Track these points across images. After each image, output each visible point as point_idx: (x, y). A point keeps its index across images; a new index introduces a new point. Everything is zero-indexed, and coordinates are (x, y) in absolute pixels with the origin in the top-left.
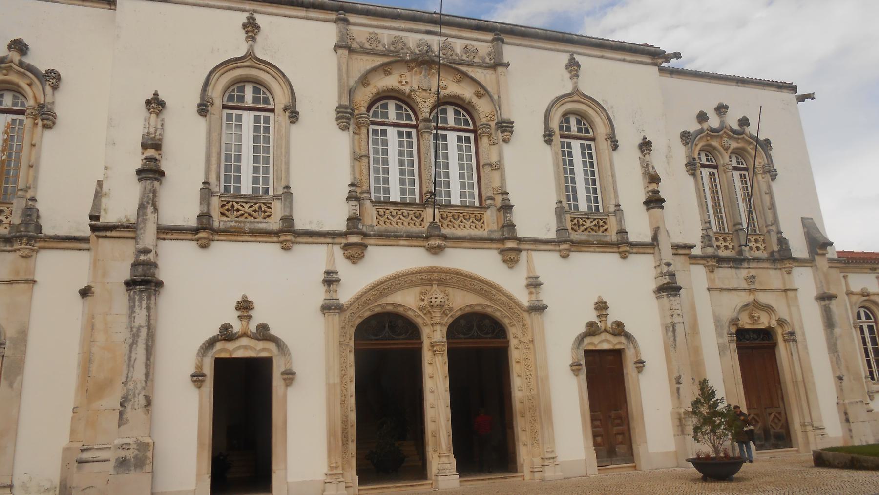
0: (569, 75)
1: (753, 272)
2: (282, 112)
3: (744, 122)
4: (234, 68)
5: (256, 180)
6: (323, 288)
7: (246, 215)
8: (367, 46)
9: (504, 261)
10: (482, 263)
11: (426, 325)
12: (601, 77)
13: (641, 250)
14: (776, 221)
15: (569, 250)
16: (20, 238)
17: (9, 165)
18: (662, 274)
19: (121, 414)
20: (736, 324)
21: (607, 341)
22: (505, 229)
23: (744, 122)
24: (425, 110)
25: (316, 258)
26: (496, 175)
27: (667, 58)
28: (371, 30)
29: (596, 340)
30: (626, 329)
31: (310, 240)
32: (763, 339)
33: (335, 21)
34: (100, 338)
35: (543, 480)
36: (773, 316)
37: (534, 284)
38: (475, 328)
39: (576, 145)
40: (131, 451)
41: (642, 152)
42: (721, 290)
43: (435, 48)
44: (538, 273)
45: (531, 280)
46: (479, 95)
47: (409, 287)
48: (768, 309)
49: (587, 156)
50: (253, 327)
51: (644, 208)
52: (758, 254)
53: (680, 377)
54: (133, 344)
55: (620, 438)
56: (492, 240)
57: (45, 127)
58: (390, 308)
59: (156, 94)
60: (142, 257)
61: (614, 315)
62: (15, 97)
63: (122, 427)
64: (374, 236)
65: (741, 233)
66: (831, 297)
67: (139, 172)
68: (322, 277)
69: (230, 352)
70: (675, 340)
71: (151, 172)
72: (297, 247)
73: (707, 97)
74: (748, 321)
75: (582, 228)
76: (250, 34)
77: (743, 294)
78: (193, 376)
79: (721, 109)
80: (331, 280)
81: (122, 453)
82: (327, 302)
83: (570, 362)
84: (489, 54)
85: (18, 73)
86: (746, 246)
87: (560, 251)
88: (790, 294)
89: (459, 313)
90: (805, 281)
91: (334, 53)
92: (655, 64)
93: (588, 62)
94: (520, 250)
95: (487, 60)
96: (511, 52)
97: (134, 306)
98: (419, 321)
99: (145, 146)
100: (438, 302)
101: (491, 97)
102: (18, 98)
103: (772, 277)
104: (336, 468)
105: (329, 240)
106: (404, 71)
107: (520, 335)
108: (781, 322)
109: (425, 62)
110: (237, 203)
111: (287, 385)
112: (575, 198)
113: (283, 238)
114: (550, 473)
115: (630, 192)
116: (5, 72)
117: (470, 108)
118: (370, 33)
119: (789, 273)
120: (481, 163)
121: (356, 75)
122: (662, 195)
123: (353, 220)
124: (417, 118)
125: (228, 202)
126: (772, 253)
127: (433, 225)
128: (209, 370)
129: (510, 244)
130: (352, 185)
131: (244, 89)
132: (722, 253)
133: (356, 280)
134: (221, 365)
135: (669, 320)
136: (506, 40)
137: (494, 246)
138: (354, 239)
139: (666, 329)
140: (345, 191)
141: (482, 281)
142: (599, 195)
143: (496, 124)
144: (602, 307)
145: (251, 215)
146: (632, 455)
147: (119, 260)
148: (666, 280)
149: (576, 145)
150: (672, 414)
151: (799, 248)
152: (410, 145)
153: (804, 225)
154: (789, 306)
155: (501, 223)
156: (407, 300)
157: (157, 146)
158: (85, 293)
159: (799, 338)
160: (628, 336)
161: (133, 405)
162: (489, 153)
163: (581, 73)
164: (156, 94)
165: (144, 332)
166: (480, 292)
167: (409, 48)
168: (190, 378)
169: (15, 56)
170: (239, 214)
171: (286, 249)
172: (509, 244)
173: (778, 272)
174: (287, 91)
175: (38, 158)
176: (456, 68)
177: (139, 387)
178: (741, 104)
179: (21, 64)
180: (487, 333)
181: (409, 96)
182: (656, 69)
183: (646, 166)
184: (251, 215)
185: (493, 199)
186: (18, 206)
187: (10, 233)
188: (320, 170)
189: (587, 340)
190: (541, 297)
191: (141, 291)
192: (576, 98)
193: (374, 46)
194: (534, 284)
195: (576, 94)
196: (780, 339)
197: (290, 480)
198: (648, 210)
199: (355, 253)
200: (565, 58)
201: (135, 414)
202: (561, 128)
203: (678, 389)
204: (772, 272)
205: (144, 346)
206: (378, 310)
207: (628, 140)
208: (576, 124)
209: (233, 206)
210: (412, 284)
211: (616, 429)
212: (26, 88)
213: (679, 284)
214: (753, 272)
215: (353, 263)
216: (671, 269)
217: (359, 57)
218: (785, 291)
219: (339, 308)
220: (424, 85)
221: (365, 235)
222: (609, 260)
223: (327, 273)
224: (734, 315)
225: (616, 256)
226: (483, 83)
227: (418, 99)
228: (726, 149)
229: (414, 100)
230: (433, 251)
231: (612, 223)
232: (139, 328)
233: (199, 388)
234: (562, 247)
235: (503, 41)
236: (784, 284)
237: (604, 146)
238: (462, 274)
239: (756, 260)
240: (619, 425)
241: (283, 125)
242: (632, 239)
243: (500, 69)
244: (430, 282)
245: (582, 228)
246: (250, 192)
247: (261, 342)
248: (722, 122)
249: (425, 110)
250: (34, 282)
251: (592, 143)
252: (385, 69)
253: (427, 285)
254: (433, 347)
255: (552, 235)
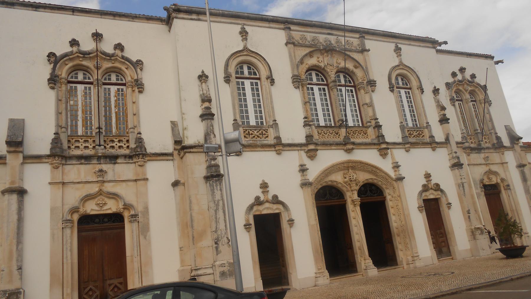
0: (396, 55)
1: (487, 155)
2: (266, 80)
3: (473, 76)
4: (239, 56)
5: (256, 117)
6: (299, 174)
7: (256, 137)
8: (301, 42)
9: (381, 155)
10: (369, 156)
11: (348, 191)
12: (412, 55)
13: (441, 146)
14: (494, 128)
15: (410, 147)
16: (138, 155)
17: (120, 115)
18: (453, 158)
19: (217, 248)
20: (482, 182)
21: (432, 194)
22: (380, 138)
23: (473, 76)
24: (332, 75)
25: (293, 159)
26: (370, 110)
27: (440, 44)
28: (301, 33)
29: (427, 193)
30: (279, 199)
31: (290, 148)
32: (114, 222)
33: (284, 29)
34: (195, 207)
35: (415, 268)
36: (498, 177)
37: (396, 166)
38: (369, 191)
39: (247, 83)
40: (226, 267)
41: (434, 95)
42: (474, 165)
43: (333, 42)
44: (397, 161)
45: (395, 164)
46: (356, 67)
47: (338, 171)
48: (496, 173)
49: (255, 89)
50: (270, 197)
51: (439, 124)
52: (487, 145)
53: (469, 210)
54: (216, 211)
55: (443, 244)
56: (374, 144)
57: (141, 92)
58: (330, 183)
59: (203, 72)
60: (213, 162)
61: (272, 191)
62: (84, 74)
63: (219, 255)
64: (321, 145)
65: (479, 134)
66: (524, 166)
67: (201, 116)
68: (298, 169)
69: (261, 211)
70: (464, 191)
71: (207, 116)
72: (283, 153)
73: (456, 63)
74: (487, 180)
75: (413, 136)
76: (244, 37)
77: (483, 166)
78: (245, 225)
79: (462, 70)
80: (303, 170)
81: (222, 269)
82: (304, 181)
83: (417, 206)
84: (359, 45)
85: (121, 62)
86: (482, 141)
87: (405, 148)
88: (505, 165)
89: (362, 184)
90: (510, 157)
91: (285, 46)
92: (434, 48)
93: (405, 48)
94: (317, 150)
95: (358, 48)
96: (369, 44)
97: (214, 189)
98: (344, 189)
99: (203, 101)
100: (354, 179)
101: (363, 68)
102: (118, 76)
103: (495, 157)
104: (321, 269)
105: (299, 148)
106: (319, 55)
107: (392, 193)
108: (503, 180)
109: (329, 50)
110: (251, 130)
111: (291, 227)
112: (248, 117)
113: (277, 148)
114: (418, 264)
115: (432, 116)
116: (113, 62)
117: (351, 74)
118: (301, 35)
119: (503, 154)
120: (361, 104)
121: (298, 59)
122: (448, 116)
123: (309, 137)
124: (327, 81)
125: (246, 130)
126: (493, 145)
127: (347, 138)
128: (252, 221)
129: (384, 146)
130: (305, 118)
131: (246, 68)
132: (472, 146)
133: (315, 169)
134: (256, 217)
135: (460, 181)
136: (366, 37)
137: (376, 147)
138: (312, 147)
139: (459, 186)
140: (302, 121)
141: (373, 166)
142: (417, 118)
143: (367, 82)
144: (428, 176)
145: (258, 137)
146: (450, 252)
147: (198, 164)
148: (456, 161)
149: (247, 83)
150: (466, 230)
151: (506, 142)
152: (325, 95)
153: (506, 129)
154: (505, 172)
155: (377, 134)
156: (338, 178)
157: (210, 101)
158: (176, 184)
159: (511, 187)
160: (442, 191)
161: (222, 243)
162: (365, 98)
163: (248, 38)
164: (203, 72)
165: (221, 203)
166: (370, 172)
167: (320, 43)
168: (243, 227)
169: (118, 52)
170: (258, 136)
171: (279, 154)
172: (382, 146)
173: (498, 154)
174: (267, 69)
175: (138, 111)
176: (344, 53)
177: (223, 233)
178: (473, 67)
179: (123, 57)
180: (374, 194)
181: (324, 69)
182: (434, 51)
183: (438, 102)
184: (258, 137)
185: (370, 122)
186: (132, 138)
187: (131, 153)
188: (289, 110)
189: (424, 194)
190: (401, 172)
191: (216, 181)
192: (401, 67)
193: (304, 42)
194: (396, 166)
195: (401, 65)
196: (502, 189)
197: (299, 278)
198: (441, 125)
199: (312, 155)
200: (238, 28)
201: (225, 249)
202: (237, 72)
203: (469, 217)
204: (495, 154)
205: (222, 211)
206: (324, 184)
207: (428, 89)
208: (403, 80)
209: (249, 132)
210: (340, 170)
211: (441, 239)
212: (125, 70)
213: (462, 162)
214: (487, 155)
215: (312, 160)
216: (457, 154)
217: (298, 48)
218: (502, 163)
219: (310, 184)
220: (330, 63)
221: (316, 144)
222: (269, 156)
223: (301, 166)
224: (481, 177)
225: (430, 150)
226: (359, 61)
227: (328, 70)
228: (466, 91)
229: (325, 71)
230: (348, 151)
231: (426, 132)
232: (218, 201)
233: (249, 232)
234: (407, 146)
235: (364, 37)
236: (63, 179)
237: (417, 92)
238: (363, 163)
239: (488, 148)
240: (442, 237)
241: (267, 86)
242: (437, 140)
243: (365, 53)
244: (348, 168)
245: (413, 136)
246: (255, 124)
247: (275, 205)
248: (463, 77)
249: (332, 75)
250: (147, 179)
251: (258, 81)
252: (310, 55)
253: (346, 169)
254: (354, 202)
255: (400, 140)
